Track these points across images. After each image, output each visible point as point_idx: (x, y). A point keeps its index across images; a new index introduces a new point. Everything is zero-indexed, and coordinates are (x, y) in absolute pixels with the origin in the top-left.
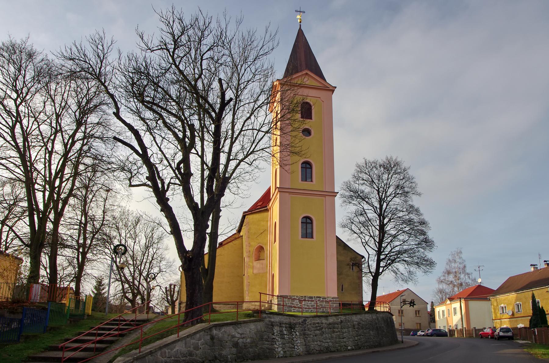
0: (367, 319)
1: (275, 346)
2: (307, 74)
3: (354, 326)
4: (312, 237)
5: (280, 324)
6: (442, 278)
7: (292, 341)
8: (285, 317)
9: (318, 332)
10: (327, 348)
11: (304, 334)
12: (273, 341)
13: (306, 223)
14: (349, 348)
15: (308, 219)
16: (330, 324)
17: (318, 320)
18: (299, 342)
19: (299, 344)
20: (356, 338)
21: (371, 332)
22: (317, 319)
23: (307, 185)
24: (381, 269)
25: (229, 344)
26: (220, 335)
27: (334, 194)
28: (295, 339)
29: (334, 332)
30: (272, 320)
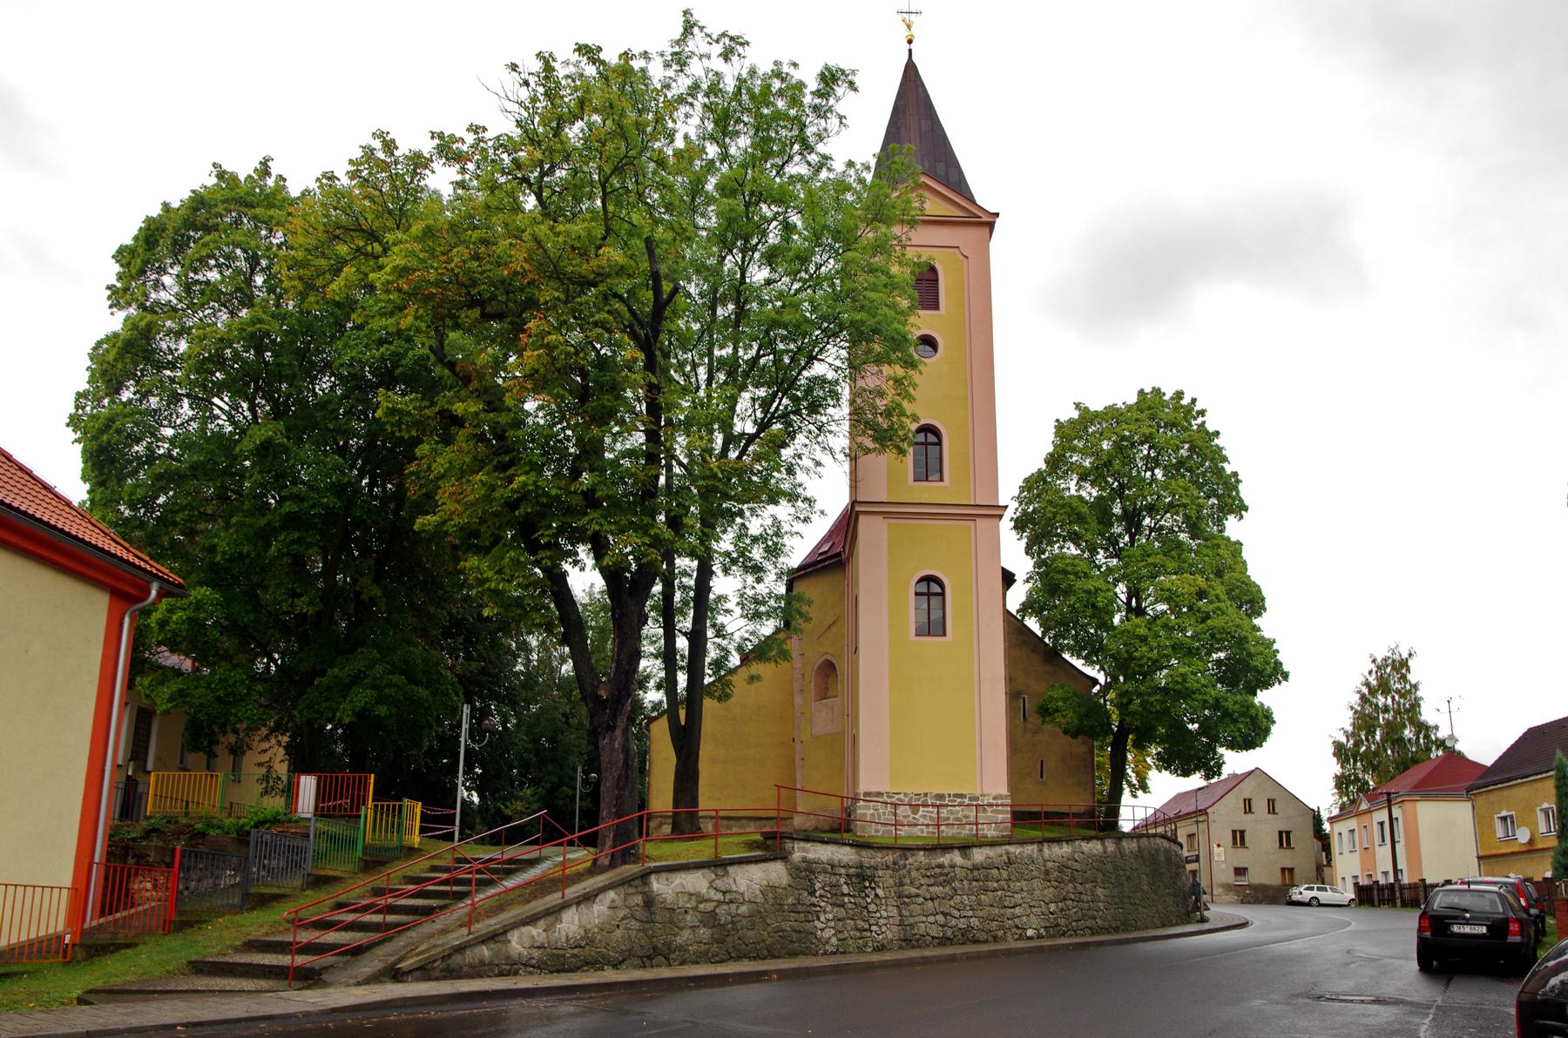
10: (964, 932)
13: (929, 594)
14: (1030, 933)
16: (976, 868)
18: (884, 914)
19: (882, 921)
20: (1053, 907)
21: (1099, 891)
23: (929, 492)
27: (997, 512)
28: (872, 907)
30: (811, 856)
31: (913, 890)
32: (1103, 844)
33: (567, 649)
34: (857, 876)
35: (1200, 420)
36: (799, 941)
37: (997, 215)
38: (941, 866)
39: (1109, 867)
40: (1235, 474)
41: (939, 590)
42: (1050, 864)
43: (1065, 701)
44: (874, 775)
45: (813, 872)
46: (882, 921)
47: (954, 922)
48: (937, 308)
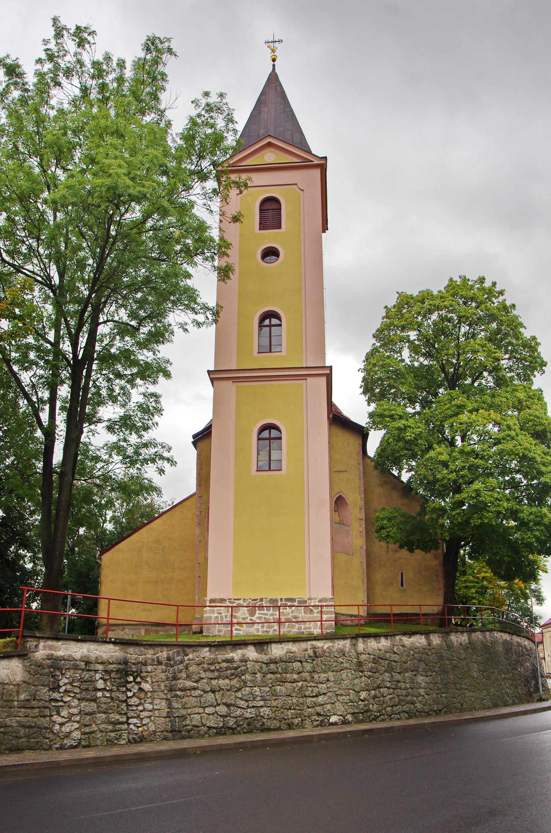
1: (56, 718)
10: (250, 722)
14: (333, 719)
15: (273, 431)
16: (274, 661)
18: (149, 706)
20: (363, 695)
21: (420, 679)
31: (189, 684)
32: (428, 638)
34: (118, 671)
35: (501, 299)
36: (28, 736)
38: (230, 661)
39: (433, 658)
40: (534, 338)
42: (363, 657)
43: (389, 520)
44: (220, 583)
45: (60, 669)
46: (146, 714)
47: (239, 712)
48: (280, 227)
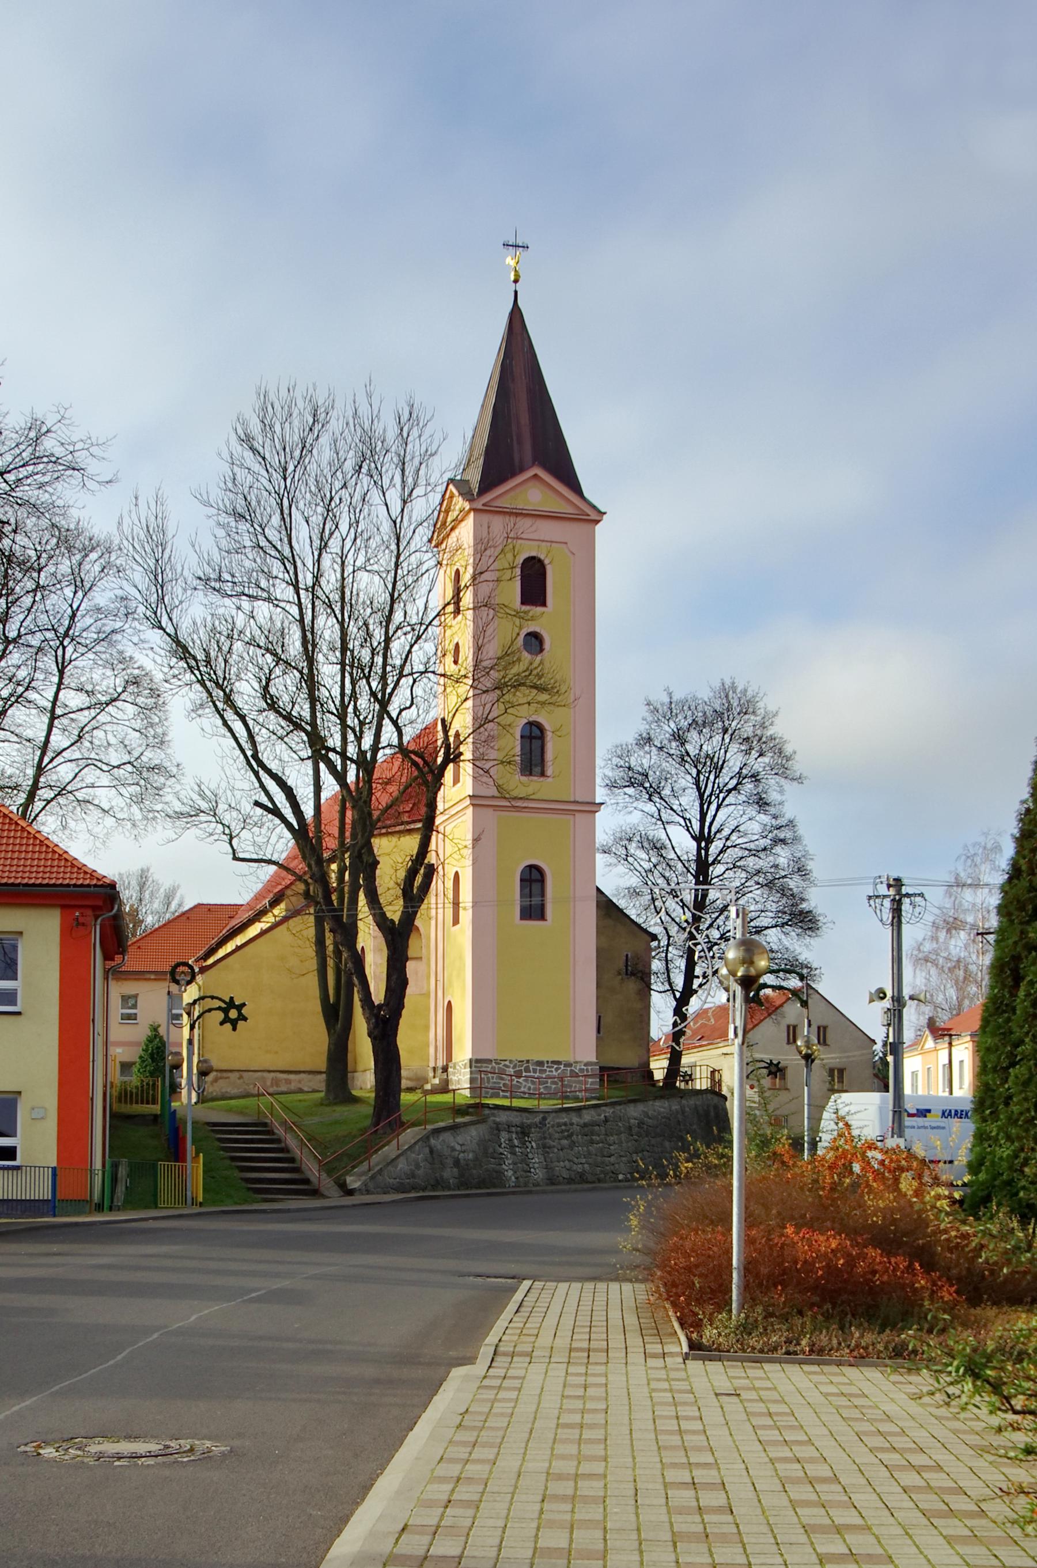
0: (659, 1113)
2: (536, 476)
3: (630, 1128)
4: (542, 917)
5: (509, 1126)
6: (928, 947)
7: (525, 1159)
8: (515, 1113)
9: (565, 1142)
11: (544, 1146)
12: (500, 1158)
14: (621, 1177)
16: (585, 1125)
17: (564, 1118)
19: (536, 1165)
22: (564, 1115)
23: (532, 786)
24: (696, 983)
25: (450, 1162)
26: (439, 1147)
28: (530, 1156)
29: (592, 1142)
30: (498, 1119)
33: (678, 1084)
37: (605, 513)
41: (539, 877)
